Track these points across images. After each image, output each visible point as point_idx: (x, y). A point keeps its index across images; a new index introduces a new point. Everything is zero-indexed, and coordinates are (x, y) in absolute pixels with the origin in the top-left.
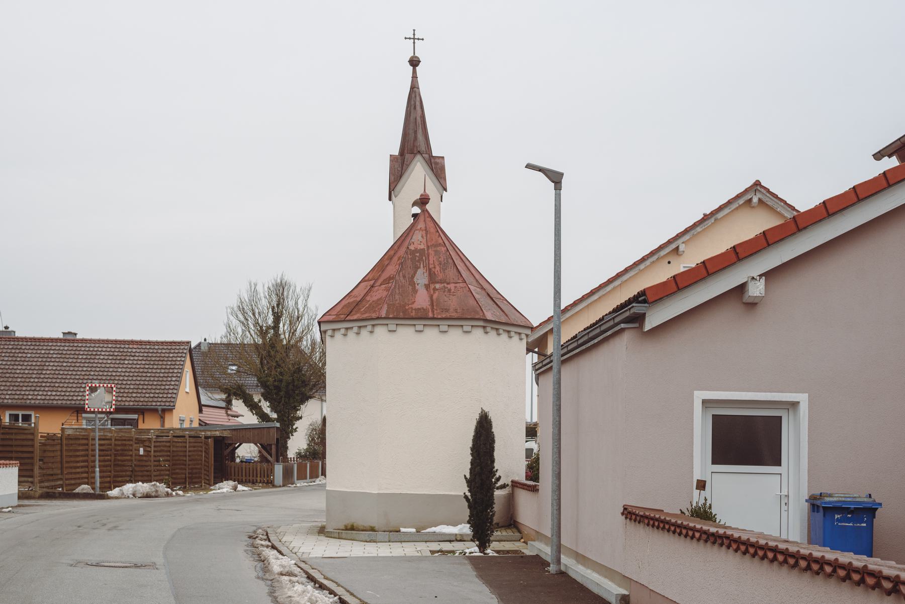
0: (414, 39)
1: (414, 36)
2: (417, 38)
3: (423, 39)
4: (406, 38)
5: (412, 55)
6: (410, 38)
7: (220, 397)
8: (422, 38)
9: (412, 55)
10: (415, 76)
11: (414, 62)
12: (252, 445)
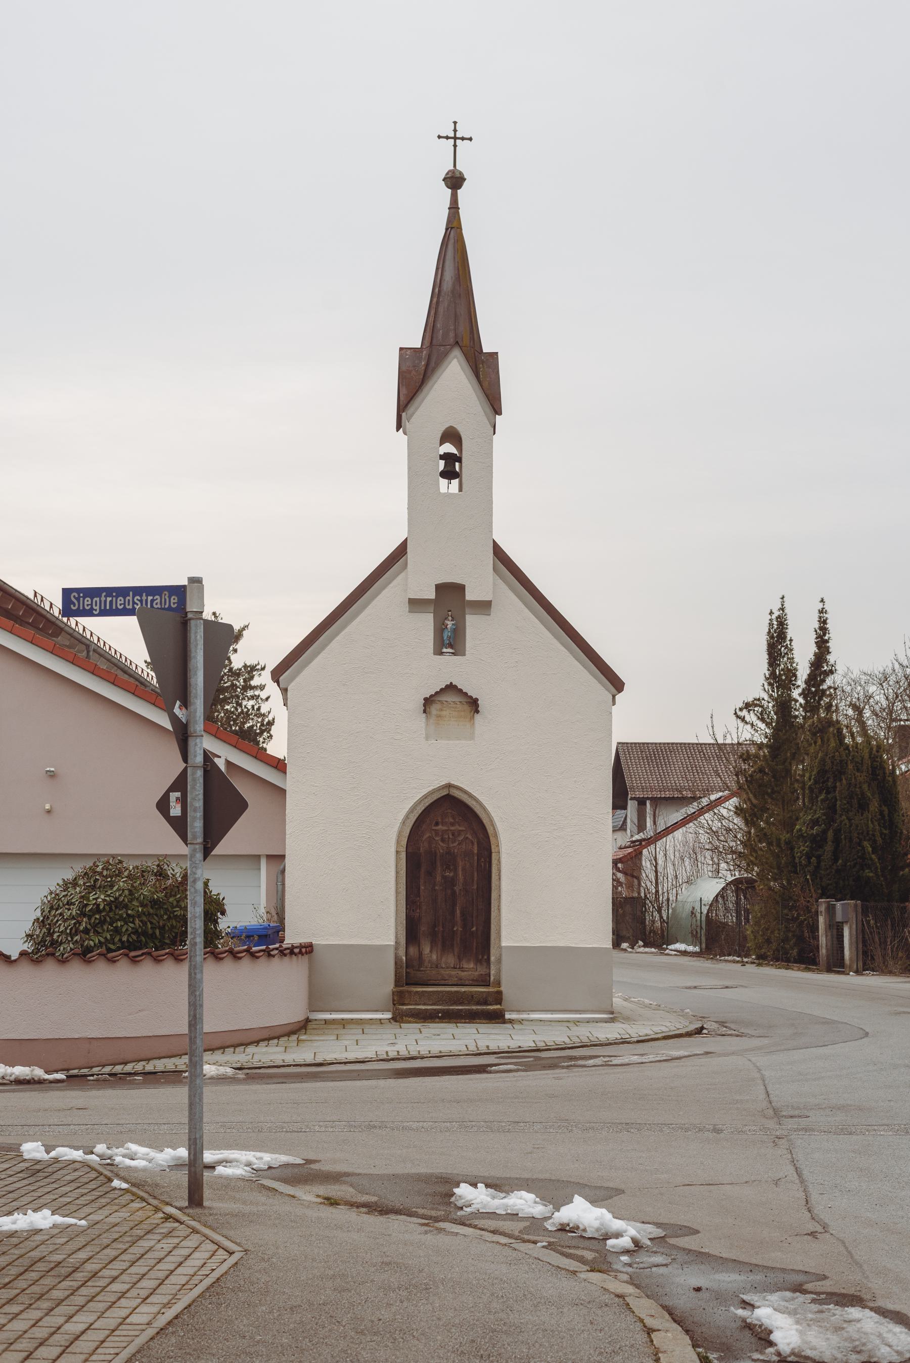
0: (455, 138)
1: (455, 134)
2: (461, 136)
3: (455, 123)
4: (439, 137)
5: (452, 168)
6: (447, 138)
7: (721, 984)
8: (453, 124)
9: (452, 168)
10: (454, 207)
11: (454, 181)
12: (524, 1193)
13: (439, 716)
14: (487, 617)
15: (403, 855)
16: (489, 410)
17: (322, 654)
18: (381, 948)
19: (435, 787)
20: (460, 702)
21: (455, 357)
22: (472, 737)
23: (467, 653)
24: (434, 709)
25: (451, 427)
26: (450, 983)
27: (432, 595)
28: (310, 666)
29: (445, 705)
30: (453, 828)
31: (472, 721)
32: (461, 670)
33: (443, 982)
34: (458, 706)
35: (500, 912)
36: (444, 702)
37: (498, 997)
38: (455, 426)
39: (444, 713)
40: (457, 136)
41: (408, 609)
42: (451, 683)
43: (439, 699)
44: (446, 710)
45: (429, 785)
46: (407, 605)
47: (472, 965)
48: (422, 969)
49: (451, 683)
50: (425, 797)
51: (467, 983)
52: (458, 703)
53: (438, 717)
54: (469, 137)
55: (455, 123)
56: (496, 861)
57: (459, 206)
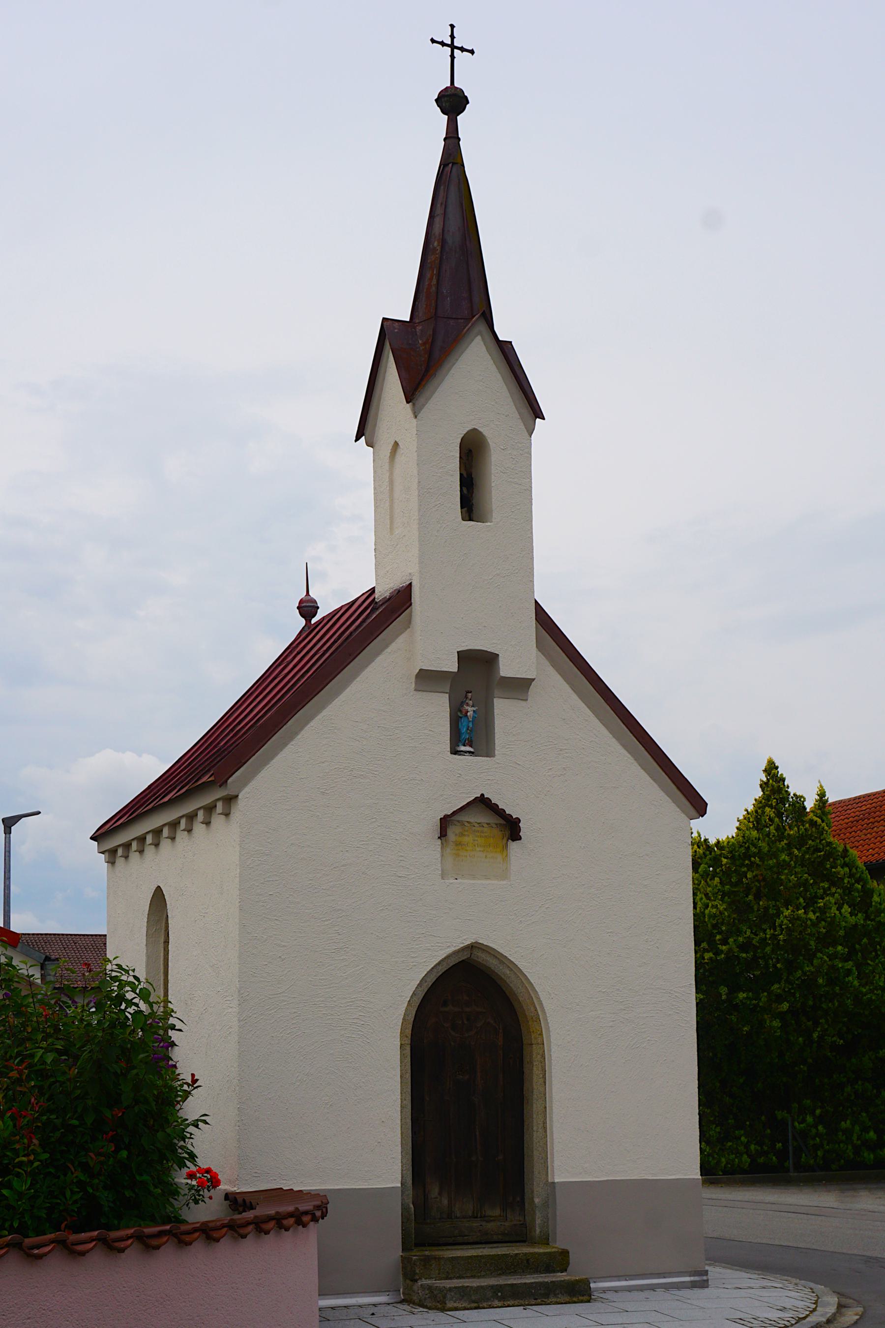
3: (452, 26)
5: (449, 85)
9: (449, 85)
10: (452, 138)
13: (458, 844)
14: (523, 703)
15: (408, 1048)
16: (527, 412)
17: (289, 746)
18: (398, 1187)
19: (457, 948)
20: (488, 824)
21: (480, 333)
22: (504, 875)
23: (496, 752)
24: (453, 832)
25: (475, 430)
26: (471, 1241)
27: (452, 666)
28: (272, 763)
29: (467, 828)
30: (468, 1010)
31: (505, 854)
32: (490, 778)
33: (460, 1239)
34: (485, 830)
35: (546, 1131)
36: (466, 824)
37: (561, 1260)
38: (480, 429)
39: (465, 839)
40: (456, 44)
41: (413, 686)
42: (482, 795)
43: (458, 819)
44: (468, 836)
45: (449, 944)
46: (413, 680)
47: (497, 1212)
48: (428, 1221)
49: (482, 795)
50: (448, 957)
51: (495, 1238)
52: (485, 825)
53: (457, 845)
54: (471, 49)
55: (452, 26)
56: (539, 1057)
57: (460, 136)
